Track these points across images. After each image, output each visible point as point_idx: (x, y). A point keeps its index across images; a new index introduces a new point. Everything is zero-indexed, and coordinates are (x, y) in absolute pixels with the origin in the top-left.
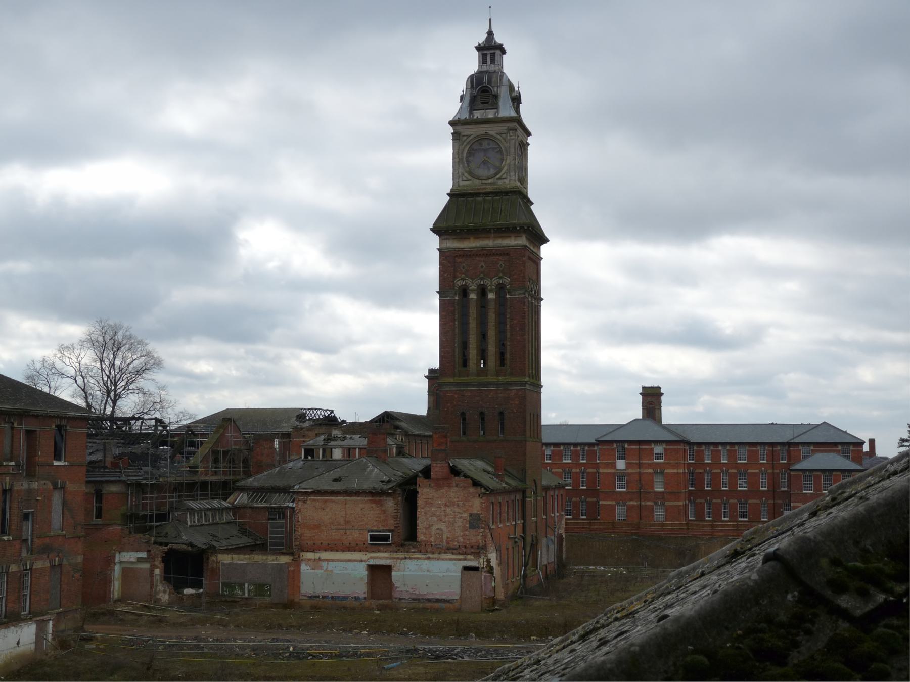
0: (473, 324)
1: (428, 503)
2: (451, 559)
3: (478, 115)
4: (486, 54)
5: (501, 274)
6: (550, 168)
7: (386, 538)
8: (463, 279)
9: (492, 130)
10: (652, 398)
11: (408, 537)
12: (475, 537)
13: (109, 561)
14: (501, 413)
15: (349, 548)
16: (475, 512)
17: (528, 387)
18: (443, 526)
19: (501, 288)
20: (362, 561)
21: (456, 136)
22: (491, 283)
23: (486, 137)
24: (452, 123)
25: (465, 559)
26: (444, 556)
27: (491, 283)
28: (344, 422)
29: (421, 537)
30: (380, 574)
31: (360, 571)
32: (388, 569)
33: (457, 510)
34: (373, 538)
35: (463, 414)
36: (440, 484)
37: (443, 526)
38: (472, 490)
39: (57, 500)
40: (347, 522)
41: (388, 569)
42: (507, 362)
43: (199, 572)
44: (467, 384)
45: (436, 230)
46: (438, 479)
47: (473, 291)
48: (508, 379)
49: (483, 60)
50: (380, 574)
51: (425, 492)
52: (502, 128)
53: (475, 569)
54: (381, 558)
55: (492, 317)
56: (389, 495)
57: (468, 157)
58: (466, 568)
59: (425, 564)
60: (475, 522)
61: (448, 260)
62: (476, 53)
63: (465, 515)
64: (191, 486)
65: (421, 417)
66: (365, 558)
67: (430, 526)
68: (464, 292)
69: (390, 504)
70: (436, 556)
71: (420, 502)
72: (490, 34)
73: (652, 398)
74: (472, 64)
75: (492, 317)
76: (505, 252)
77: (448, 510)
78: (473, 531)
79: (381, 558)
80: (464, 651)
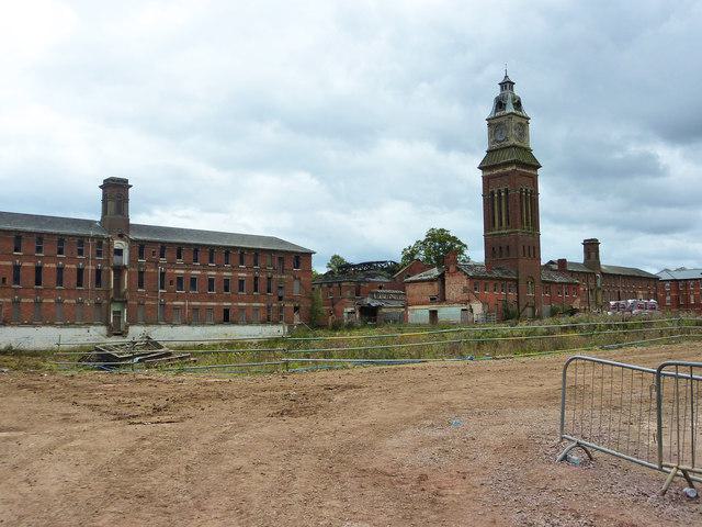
0: (496, 207)
3: (498, 114)
6: (542, 138)
9: (502, 120)
10: (116, 191)
11: (441, 298)
13: (343, 312)
19: (507, 191)
21: (489, 125)
22: (502, 189)
23: (500, 124)
27: (502, 189)
28: (410, 255)
30: (433, 314)
31: (427, 313)
32: (436, 311)
36: (452, 274)
39: (296, 284)
41: (436, 311)
43: (375, 315)
45: (480, 168)
49: (502, 89)
50: (433, 314)
61: (486, 180)
62: (499, 87)
65: (534, 249)
68: (493, 193)
72: (506, 77)
73: (116, 191)
74: (497, 92)
76: (507, 174)
79: (434, 307)
80: (633, 305)
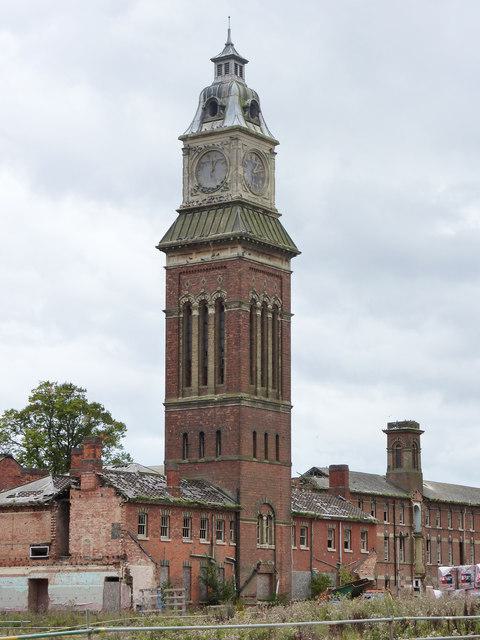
1: (79, 515)
2: (96, 570)
3: (207, 127)
4: (221, 65)
5: (219, 289)
7: (43, 552)
8: (187, 296)
11: (58, 550)
12: (116, 548)
14: (219, 433)
15: (15, 563)
16: (117, 521)
17: (244, 403)
18: (89, 537)
20: (24, 575)
21: (187, 151)
22: (211, 300)
24: (183, 139)
25: (107, 570)
26: (90, 567)
27: (211, 300)
29: (72, 550)
31: (22, 587)
33: (102, 520)
34: (35, 552)
35: (185, 435)
37: (89, 537)
38: (114, 499)
40: (14, 537)
42: (225, 379)
44: (189, 404)
45: (161, 248)
46: (87, 491)
47: (195, 308)
48: (225, 395)
50: (39, 587)
51: (76, 504)
52: (225, 138)
53: (115, 579)
54: (39, 571)
55: (211, 332)
56: (47, 508)
57: (197, 171)
58: (109, 579)
59: (76, 577)
60: (116, 532)
63: (109, 525)
64: (412, 566)
66: (27, 572)
67: (80, 538)
68: (188, 308)
69: (48, 518)
70: (84, 568)
71: (72, 513)
72: (229, 45)
75: (211, 332)
76: (222, 265)
77: (95, 520)
78: (114, 541)
79: (39, 571)
